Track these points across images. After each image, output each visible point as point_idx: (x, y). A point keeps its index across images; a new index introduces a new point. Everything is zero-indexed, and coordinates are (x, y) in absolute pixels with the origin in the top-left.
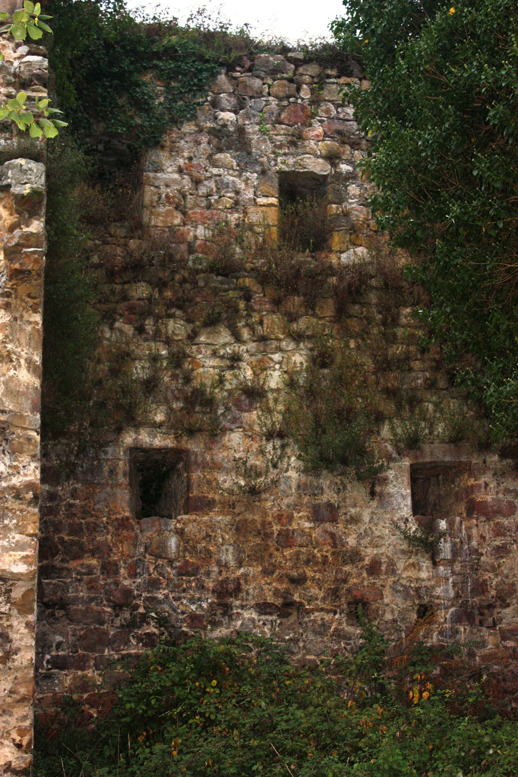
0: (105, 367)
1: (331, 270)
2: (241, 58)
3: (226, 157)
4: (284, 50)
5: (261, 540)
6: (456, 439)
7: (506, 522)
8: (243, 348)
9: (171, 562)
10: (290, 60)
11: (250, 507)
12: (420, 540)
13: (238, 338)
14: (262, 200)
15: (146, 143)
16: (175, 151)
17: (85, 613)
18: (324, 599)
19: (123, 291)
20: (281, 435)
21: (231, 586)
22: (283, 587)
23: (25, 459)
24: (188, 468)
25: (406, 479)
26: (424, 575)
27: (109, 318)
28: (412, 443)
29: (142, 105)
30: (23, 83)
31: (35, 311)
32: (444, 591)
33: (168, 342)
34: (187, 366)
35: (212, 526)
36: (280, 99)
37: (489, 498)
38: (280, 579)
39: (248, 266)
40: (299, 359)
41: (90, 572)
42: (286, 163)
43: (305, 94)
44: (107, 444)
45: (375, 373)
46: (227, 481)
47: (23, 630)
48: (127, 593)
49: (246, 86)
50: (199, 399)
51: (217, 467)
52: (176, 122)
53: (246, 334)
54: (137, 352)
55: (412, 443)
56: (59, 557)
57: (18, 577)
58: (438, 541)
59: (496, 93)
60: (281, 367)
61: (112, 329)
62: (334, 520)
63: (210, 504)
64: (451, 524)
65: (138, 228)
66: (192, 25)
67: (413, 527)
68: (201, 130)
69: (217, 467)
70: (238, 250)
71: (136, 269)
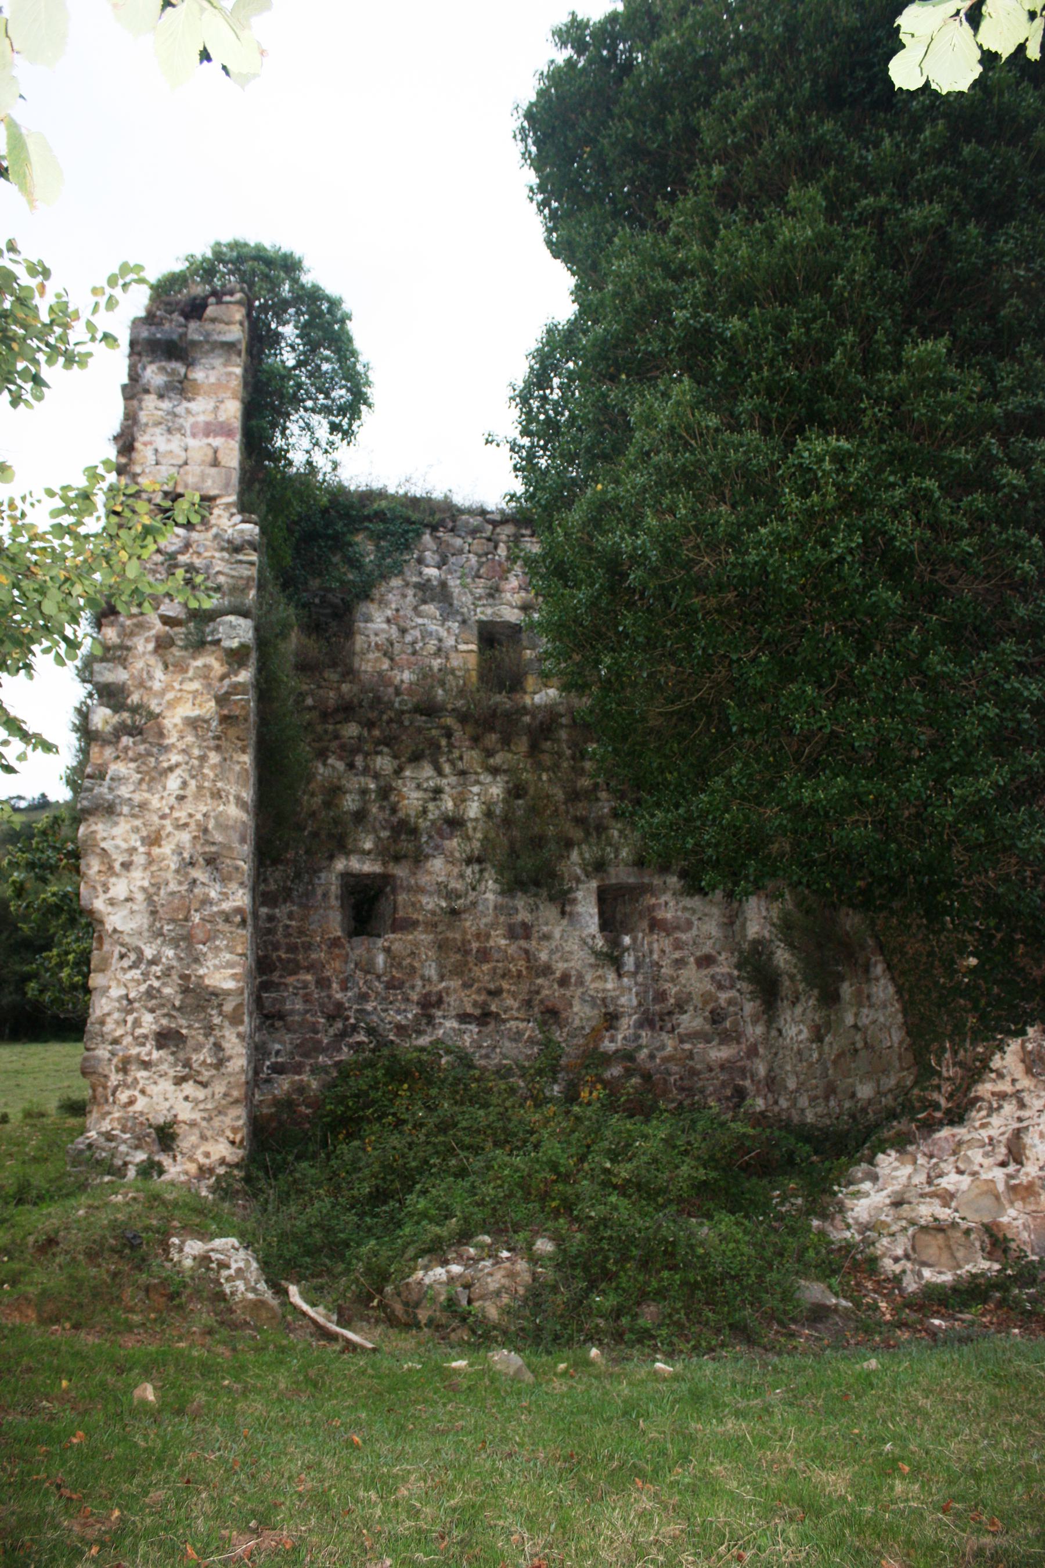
0: (318, 800)
1: (524, 710)
2: (443, 520)
3: (430, 608)
4: (483, 512)
5: (462, 957)
6: (640, 863)
7: (684, 937)
8: (445, 781)
9: (378, 977)
10: (489, 522)
11: (450, 926)
12: (606, 954)
13: (440, 773)
14: (462, 647)
15: (357, 596)
16: (383, 603)
17: (301, 1024)
18: (519, 1009)
19: (335, 731)
20: (479, 860)
21: (434, 999)
22: (481, 998)
23: (234, 886)
24: (394, 891)
25: (593, 899)
26: (609, 986)
27: (322, 755)
28: (599, 867)
29: (354, 563)
30: (236, 548)
31: (244, 752)
32: (628, 1001)
33: (376, 776)
34: (393, 798)
35: (416, 944)
36: (479, 556)
37: (669, 916)
38: (479, 991)
39: (450, 707)
40: (496, 790)
41: (305, 987)
42: (484, 613)
43: (502, 551)
44: (320, 870)
45: (565, 803)
46: (430, 903)
47: (235, 1040)
48: (339, 1005)
49: (448, 545)
50: (404, 829)
51: (421, 890)
52: (384, 577)
53: (447, 768)
54: (349, 786)
55: (599, 867)
56: (277, 974)
57: (228, 993)
58: (622, 955)
59: (635, 560)
60: (481, 796)
61: (325, 765)
62: (528, 937)
63: (415, 924)
64: (634, 940)
65: (349, 673)
66: (401, 492)
67: (600, 943)
68: (407, 584)
69: (421, 890)
70: (440, 692)
71: (347, 710)
